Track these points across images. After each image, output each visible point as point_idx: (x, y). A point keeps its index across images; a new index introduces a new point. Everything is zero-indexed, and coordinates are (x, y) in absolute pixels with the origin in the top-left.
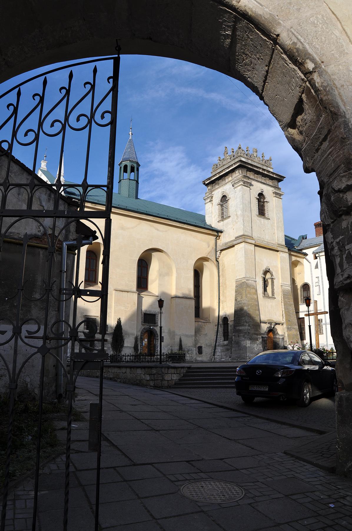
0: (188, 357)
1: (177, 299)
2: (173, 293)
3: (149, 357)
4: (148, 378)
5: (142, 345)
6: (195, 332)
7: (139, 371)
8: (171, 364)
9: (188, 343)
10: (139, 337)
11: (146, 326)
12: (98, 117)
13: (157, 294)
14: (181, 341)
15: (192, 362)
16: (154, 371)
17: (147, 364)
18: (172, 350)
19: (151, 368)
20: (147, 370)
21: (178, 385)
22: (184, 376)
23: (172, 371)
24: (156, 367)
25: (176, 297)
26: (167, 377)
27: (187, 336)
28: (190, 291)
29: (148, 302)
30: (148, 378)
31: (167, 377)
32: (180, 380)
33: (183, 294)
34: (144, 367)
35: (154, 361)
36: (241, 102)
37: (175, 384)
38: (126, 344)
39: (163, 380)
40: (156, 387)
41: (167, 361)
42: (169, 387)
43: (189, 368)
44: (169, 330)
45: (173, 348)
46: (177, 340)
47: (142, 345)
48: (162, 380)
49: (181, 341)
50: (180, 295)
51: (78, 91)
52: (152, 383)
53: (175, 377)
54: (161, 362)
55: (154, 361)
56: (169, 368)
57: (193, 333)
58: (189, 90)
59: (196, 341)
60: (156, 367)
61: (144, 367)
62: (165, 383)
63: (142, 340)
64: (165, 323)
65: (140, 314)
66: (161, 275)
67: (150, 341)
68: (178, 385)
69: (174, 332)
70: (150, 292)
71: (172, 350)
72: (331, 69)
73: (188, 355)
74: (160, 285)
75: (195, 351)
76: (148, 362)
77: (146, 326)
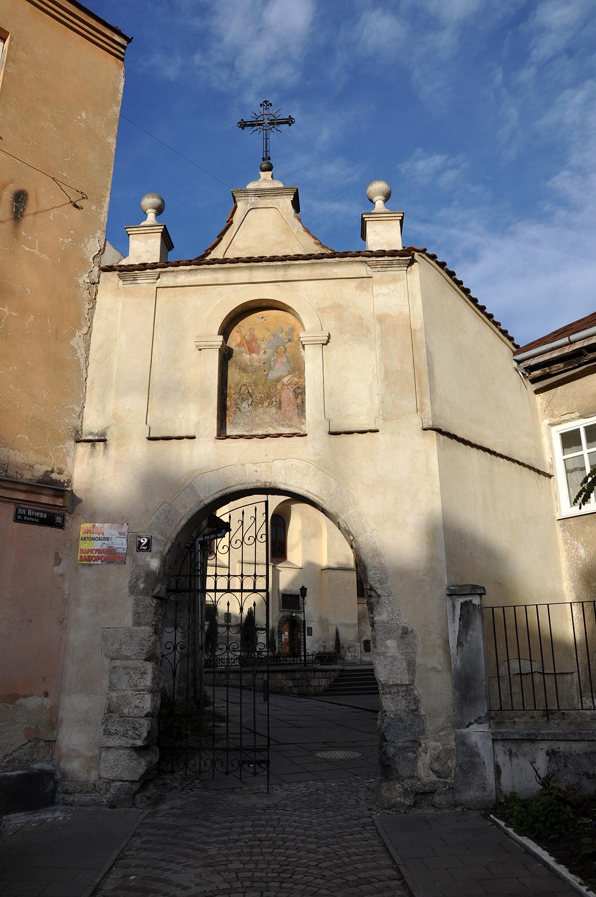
0: (349, 657)
1: (330, 571)
2: (324, 562)
3: (301, 785)
4: (290, 684)
5: (280, 641)
6: (359, 619)
7: (279, 676)
8: (319, 667)
9: (349, 635)
10: (276, 630)
11: (286, 613)
12: (259, 537)
13: (300, 565)
14: (337, 633)
15: (355, 664)
16: (298, 675)
17: (289, 668)
18: (325, 647)
19: (294, 671)
20: (288, 674)
21: (329, 691)
22: (336, 681)
23: (320, 674)
24: (300, 671)
25: (328, 569)
26: (314, 682)
27: (347, 625)
28: (348, 559)
29: (286, 578)
30: (290, 684)
31: (314, 682)
32: (330, 686)
33: (338, 563)
34: (285, 671)
35: (297, 663)
36: (424, 221)
37: (324, 691)
38: (260, 640)
39: (309, 685)
40: (300, 695)
41: (313, 663)
42: (317, 694)
43: (342, 671)
44: (320, 618)
45: (327, 644)
46: (332, 632)
47: (280, 641)
48: (307, 687)
49: (337, 633)
50: (334, 565)
51: (248, 522)
52: (295, 690)
53: (324, 682)
54: (305, 664)
55: (297, 663)
56: (316, 671)
57: (356, 621)
58: (335, 207)
59: (360, 633)
60: (300, 671)
61: (285, 671)
62: (312, 690)
63: (280, 633)
64: (311, 611)
65: (277, 596)
66: (306, 537)
67: (291, 635)
68: (329, 691)
69: (327, 620)
70: (290, 563)
71: (325, 647)
72: (360, 540)
73: (349, 654)
74: (304, 551)
75: (359, 647)
76: (290, 664)
77: (286, 613)
